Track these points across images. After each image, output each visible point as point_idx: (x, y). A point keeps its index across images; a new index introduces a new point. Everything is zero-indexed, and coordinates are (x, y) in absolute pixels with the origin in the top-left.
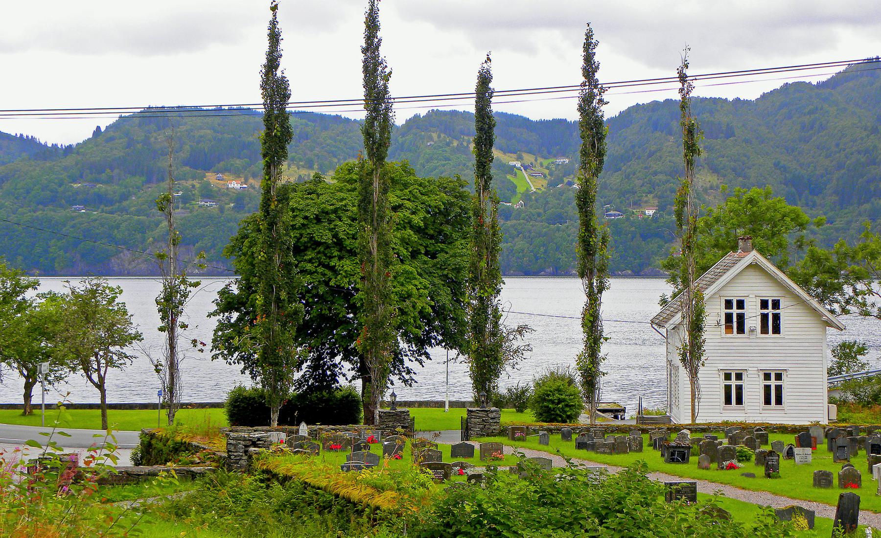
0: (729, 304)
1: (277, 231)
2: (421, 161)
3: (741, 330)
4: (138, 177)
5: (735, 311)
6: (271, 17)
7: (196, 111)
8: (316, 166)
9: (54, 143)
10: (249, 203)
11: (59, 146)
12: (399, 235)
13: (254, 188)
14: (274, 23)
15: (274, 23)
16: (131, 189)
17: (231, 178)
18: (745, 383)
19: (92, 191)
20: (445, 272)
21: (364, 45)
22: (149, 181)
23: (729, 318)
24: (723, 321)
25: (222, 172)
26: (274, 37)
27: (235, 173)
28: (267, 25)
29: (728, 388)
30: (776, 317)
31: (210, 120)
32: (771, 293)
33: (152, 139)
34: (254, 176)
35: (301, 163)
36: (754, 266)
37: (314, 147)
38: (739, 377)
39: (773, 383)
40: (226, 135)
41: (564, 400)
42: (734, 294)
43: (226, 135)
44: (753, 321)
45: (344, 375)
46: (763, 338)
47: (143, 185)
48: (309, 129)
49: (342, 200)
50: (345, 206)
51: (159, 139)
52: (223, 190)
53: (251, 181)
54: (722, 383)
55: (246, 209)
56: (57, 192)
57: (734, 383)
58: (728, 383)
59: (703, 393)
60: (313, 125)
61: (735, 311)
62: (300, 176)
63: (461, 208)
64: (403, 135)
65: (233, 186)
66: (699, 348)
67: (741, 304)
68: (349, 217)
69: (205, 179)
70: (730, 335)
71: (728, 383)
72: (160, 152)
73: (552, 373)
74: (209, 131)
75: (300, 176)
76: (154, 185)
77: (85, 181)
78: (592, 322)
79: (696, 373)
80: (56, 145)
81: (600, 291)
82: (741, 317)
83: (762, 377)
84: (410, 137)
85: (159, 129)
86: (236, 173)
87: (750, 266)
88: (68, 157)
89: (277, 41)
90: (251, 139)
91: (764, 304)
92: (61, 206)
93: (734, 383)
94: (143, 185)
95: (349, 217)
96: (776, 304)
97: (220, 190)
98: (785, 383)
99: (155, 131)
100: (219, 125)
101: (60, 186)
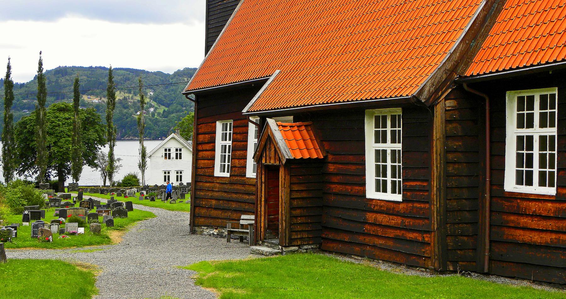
0: (166, 150)
1: (9, 128)
2: (180, 90)
3: (169, 158)
4: (52, 97)
5: (168, 152)
6: (8, 62)
7: (81, 68)
8: (132, 92)
9: (17, 82)
10: (102, 108)
11: (19, 84)
12: (67, 128)
13: (104, 102)
14: (9, 63)
15: (9, 63)
16: (49, 103)
17: (94, 97)
18: (171, 175)
19: (32, 103)
20: (84, 140)
21: (38, 70)
22: (58, 99)
23: (166, 154)
24: (164, 155)
25: (90, 95)
26: (9, 67)
27: (96, 95)
28: (7, 64)
29: (177, 176)
30: (180, 154)
31: (86, 72)
32: (179, 146)
33: (60, 81)
34: (104, 97)
35: (125, 91)
36: (173, 138)
37: (132, 84)
38: (169, 173)
39: (179, 174)
40: (92, 79)
41: (130, 183)
42: (167, 147)
43: (92, 79)
44: (173, 155)
45: (53, 175)
46: (169, 161)
47: (55, 101)
48: (130, 76)
49: (49, 116)
50: (49, 118)
51: (62, 80)
52: (90, 103)
53: (103, 99)
54: (163, 175)
55: (100, 111)
56: (16, 104)
57: (167, 175)
58: (165, 175)
59: (337, 188)
60: (132, 74)
61: (168, 152)
62: (125, 97)
63: (92, 118)
64: (172, 79)
65: (95, 101)
66: (145, 163)
67: (169, 150)
68: (50, 122)
69: (82, 98)
70: (177, 160)
71: (165, 175)
72: (62, 86)
73: (129, 175)
74: (85, 77)
75: (125, 97)
76: (60, 101)
77: (29, 99)
78: (111, 156)
79: (144, 172)
80: (18, 83)
81: (113, 147)
82: (169, 154)
83: (176, 173)
84: (175, 80)
85: (63, 76)
86: (97, 95)
87: (172, 138)
88: (22, 89)
89: (10, 69)
90: (104, 80)
91: (177, 150)
92: (18, 110)
93: (167, 175)
94: (55, 101)
95: (50, 122)
96: (180, 150)
97: (89, 103)
98: (183, 174)
99: (61, 77)
100: (90, 74)
101: (18, 101)
